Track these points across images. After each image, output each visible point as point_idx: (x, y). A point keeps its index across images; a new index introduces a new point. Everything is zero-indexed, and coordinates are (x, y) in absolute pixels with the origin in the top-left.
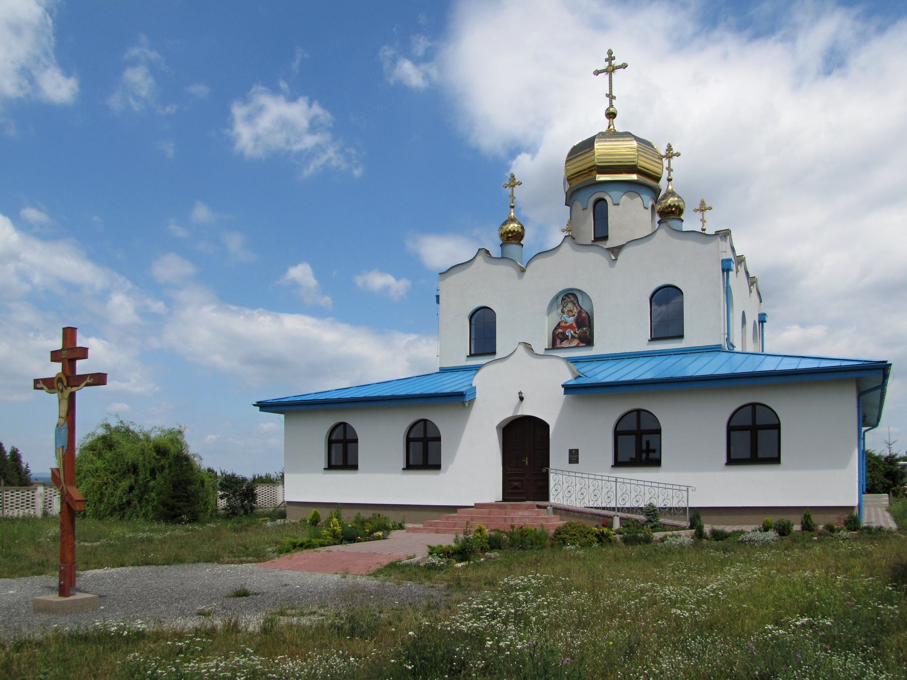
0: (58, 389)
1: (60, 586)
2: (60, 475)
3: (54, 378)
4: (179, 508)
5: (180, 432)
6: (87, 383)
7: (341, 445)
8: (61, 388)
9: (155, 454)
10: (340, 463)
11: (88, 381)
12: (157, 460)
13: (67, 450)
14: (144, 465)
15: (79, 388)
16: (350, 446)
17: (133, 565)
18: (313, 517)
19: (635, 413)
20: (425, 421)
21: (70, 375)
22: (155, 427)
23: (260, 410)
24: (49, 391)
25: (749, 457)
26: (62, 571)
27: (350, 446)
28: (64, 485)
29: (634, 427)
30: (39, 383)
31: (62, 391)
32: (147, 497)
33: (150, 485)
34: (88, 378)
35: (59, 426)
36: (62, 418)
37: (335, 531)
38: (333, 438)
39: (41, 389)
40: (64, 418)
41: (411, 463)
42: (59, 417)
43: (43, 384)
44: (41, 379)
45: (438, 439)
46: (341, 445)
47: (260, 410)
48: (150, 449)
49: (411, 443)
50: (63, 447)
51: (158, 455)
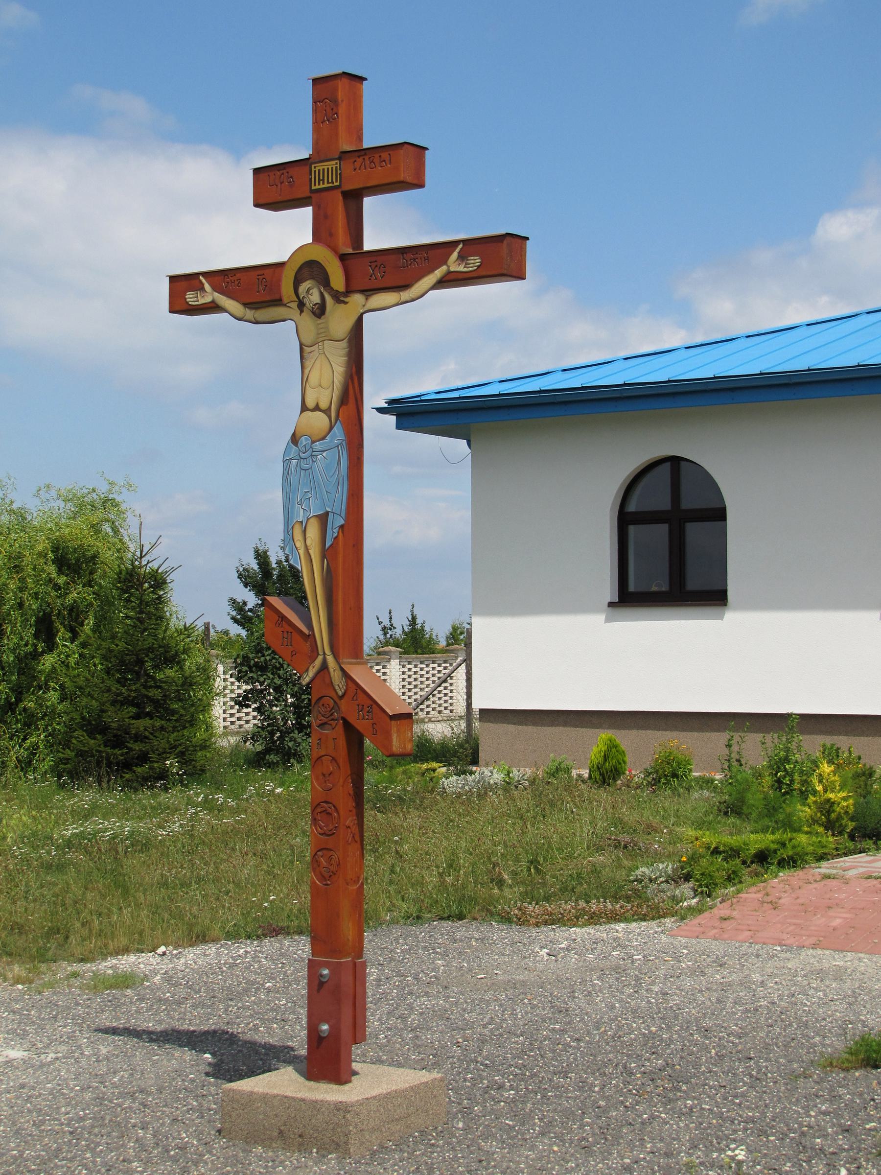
0: (301, 305)
1: (315, 1039)
2: (310, 627)
3: (281, 265)
4: (138, 738)
5: (107, 502)
6: (449, 273)
7: (661, 531)
8: (315, 298)
9: (52, 569)
10: (660, 585)
11: (454, 264)
12: (57, 587)
13: (342, 527)
14: (21, 605)
15: (405, 295)
16: (694, 532)
17: (233, 936)
18: (606, 758)
19: (667, 466)
20: (675, 461)
21: (350, 251)
22: (48, 486)
23: (399, 426)
24: (250, 314)
25: (665, 588)
26: (321, 984)
27: (694, 532)
28: (330, 659)
29: (663, 503)
30: (202, 288)
31: (320, 311)
32: (31, 705)
33: (41, 667)
34: (455, 255)
35: (304, 441)
36: (317, 408)
37: (831, 803)
38: (632, 507)
39: (213, 308)
40: (327, 412)
41: (632, 588)
42: (304, 408)
43: (215, 288)
44: (207, 274)
45: (719, 514)
46: (661, 531)
47: (399, 426)
48: (42, 555)
49: (632, 529)
50: (323, 519)
51: (60, 572)
